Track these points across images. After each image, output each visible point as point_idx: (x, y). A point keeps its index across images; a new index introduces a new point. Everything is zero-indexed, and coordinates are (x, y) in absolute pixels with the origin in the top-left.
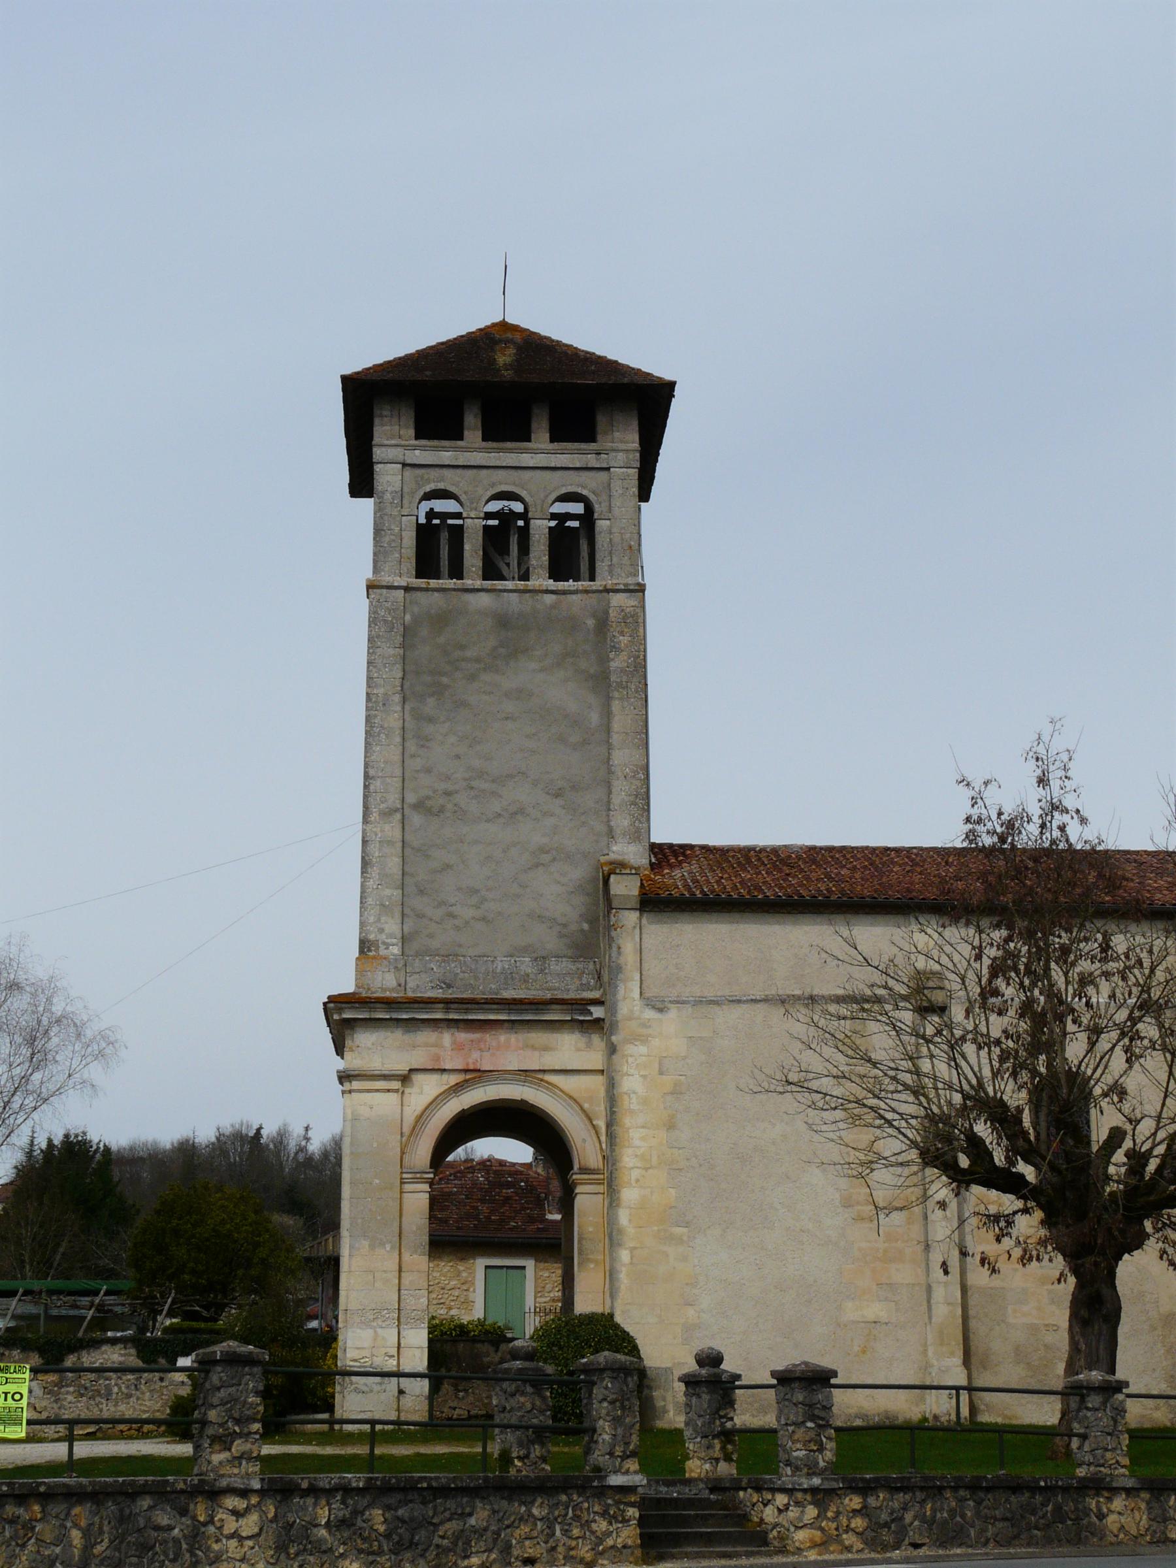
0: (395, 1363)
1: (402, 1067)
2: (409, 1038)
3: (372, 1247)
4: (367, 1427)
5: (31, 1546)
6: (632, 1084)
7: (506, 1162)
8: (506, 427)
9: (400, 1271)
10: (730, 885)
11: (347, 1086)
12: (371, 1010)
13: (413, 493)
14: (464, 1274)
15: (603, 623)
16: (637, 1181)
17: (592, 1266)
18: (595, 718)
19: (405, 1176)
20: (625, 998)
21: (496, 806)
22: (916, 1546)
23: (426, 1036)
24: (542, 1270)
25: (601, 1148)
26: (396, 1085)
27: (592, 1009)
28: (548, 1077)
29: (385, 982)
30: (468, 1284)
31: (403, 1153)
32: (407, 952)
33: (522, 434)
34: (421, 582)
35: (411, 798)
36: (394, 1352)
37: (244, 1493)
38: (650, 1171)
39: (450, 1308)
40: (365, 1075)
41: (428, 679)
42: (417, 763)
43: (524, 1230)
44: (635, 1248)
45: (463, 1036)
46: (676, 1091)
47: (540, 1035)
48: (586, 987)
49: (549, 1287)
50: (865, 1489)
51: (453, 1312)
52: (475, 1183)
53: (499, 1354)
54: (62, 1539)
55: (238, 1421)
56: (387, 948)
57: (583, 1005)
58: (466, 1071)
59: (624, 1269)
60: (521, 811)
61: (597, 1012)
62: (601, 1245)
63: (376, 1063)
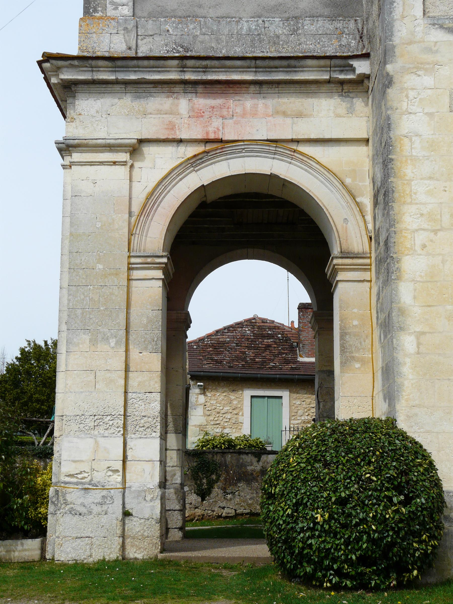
0: (120, 479)
3: (93, 342)
7: (267, 320)
9: (127, 370)
11: (68, 160)
12: (93, 69)
14: (235, 402)
16: (424, 246)
17: (357, 365)
19: (133, 260)
20: (403, 17)
23: (159, 102)
24: (296, 399)
25: (366, 228)
26: (124, 157)
27: (355, 63)
28: (302, 148)
29: (115, 43)
30: (237, 410)
31: (131, 234)
32: (139, 13)
36: (119, 465)
38: (440, 234)
39: (224, 428)
40: (86, 146)
43: (281, 369)
44: (424, 333)
45: (202, 102)
47: (292, 100)
49: (300, 412)
51: (226, 431)
52: (243, 336)
53: (261, 463)
56: (116, 8)
57: (343, 61)
58: (207, 141)
59: (408, 360)
61: (362, 67)
62: (368, 341)
63: (100, 132)
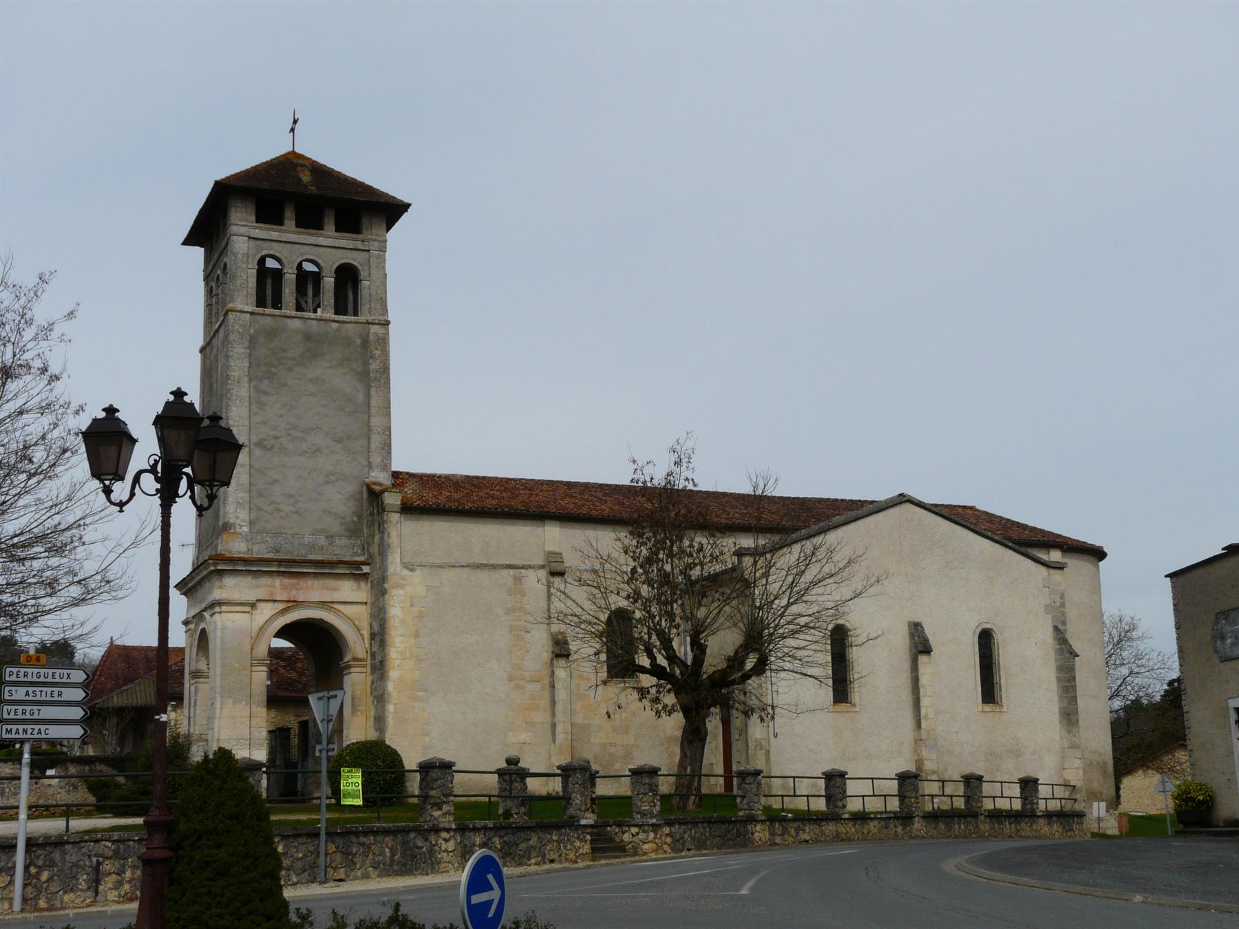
1: (252, 599)
2: (255, 582)
3: (234, 703)
4: (487, 799)
5: (370, 856)
6: (396, 610)
8: (310, 220)
10: (430, 498)
13: (254, 256)
15: (365, 343)
18: (361, 397)
21: (304, 446)
22: (689, 850)
23: (266, 580)
26: (248, 609)
28: (336, 606)
33: (319, 226)
34: (259, 310)
35: (254, 439)
37: (448, 830)
41: (264, 369)
42: (258, 419)
45: (287, 581)
46: (420, 616)
48: (356, 554)
50: (670, 823)
54: (382, 853)
55: (445, 796)
57: (358, 565)
60: (318, 450)
61: (366, 569)
